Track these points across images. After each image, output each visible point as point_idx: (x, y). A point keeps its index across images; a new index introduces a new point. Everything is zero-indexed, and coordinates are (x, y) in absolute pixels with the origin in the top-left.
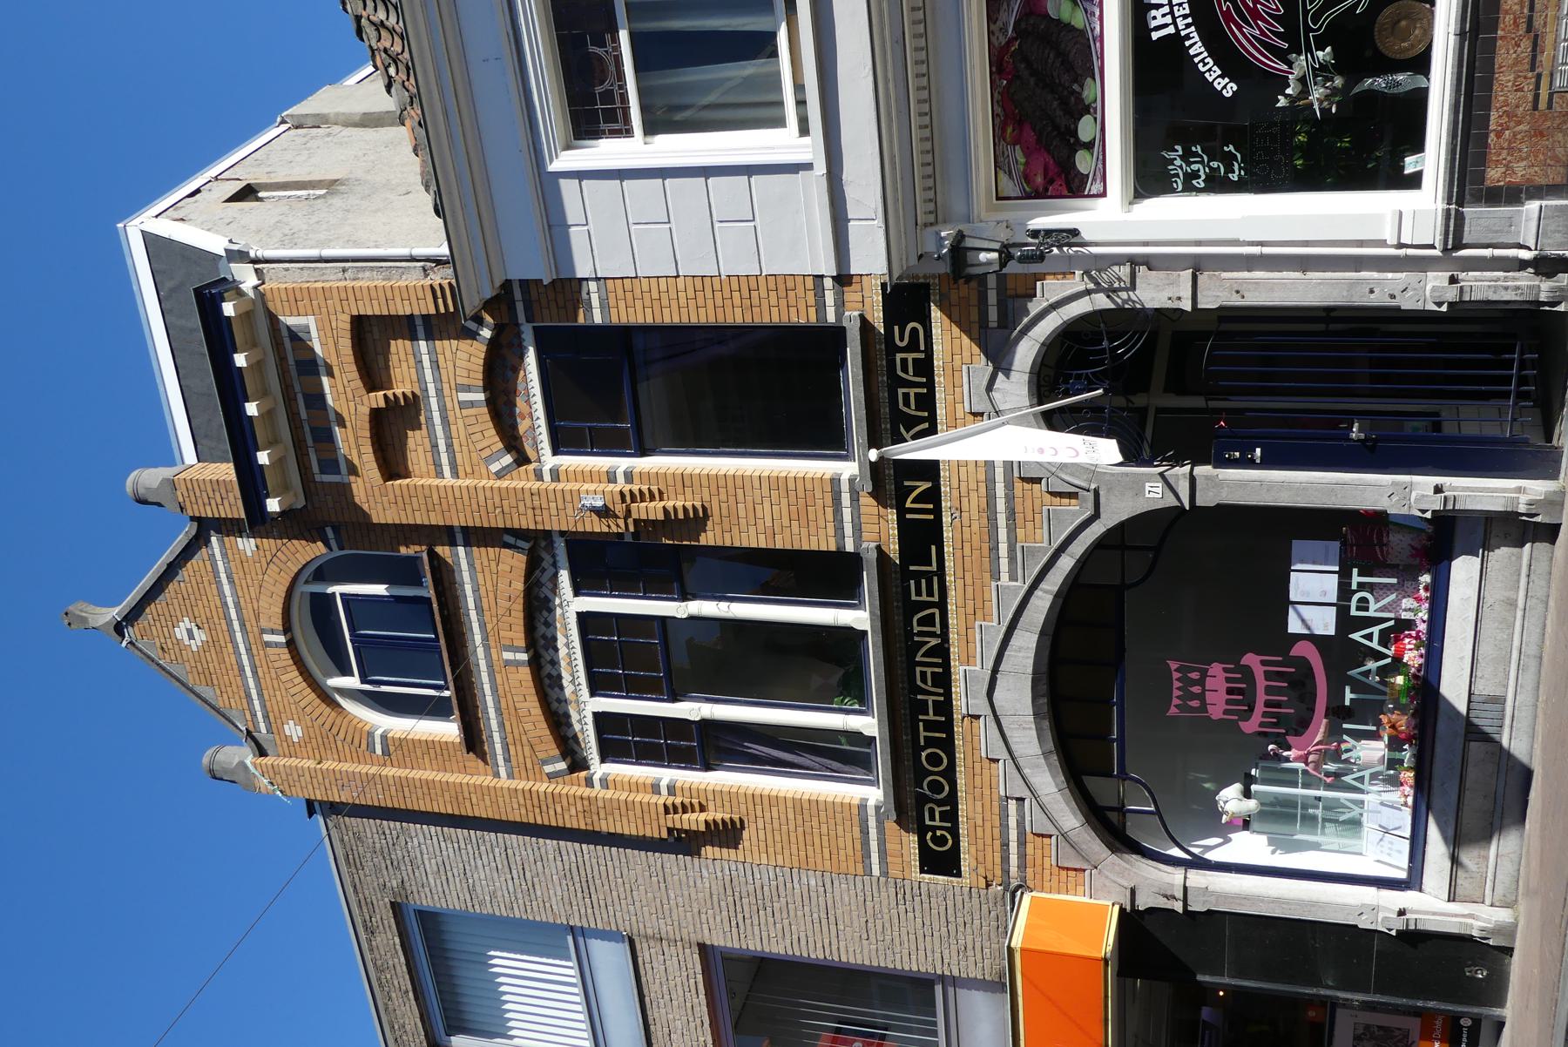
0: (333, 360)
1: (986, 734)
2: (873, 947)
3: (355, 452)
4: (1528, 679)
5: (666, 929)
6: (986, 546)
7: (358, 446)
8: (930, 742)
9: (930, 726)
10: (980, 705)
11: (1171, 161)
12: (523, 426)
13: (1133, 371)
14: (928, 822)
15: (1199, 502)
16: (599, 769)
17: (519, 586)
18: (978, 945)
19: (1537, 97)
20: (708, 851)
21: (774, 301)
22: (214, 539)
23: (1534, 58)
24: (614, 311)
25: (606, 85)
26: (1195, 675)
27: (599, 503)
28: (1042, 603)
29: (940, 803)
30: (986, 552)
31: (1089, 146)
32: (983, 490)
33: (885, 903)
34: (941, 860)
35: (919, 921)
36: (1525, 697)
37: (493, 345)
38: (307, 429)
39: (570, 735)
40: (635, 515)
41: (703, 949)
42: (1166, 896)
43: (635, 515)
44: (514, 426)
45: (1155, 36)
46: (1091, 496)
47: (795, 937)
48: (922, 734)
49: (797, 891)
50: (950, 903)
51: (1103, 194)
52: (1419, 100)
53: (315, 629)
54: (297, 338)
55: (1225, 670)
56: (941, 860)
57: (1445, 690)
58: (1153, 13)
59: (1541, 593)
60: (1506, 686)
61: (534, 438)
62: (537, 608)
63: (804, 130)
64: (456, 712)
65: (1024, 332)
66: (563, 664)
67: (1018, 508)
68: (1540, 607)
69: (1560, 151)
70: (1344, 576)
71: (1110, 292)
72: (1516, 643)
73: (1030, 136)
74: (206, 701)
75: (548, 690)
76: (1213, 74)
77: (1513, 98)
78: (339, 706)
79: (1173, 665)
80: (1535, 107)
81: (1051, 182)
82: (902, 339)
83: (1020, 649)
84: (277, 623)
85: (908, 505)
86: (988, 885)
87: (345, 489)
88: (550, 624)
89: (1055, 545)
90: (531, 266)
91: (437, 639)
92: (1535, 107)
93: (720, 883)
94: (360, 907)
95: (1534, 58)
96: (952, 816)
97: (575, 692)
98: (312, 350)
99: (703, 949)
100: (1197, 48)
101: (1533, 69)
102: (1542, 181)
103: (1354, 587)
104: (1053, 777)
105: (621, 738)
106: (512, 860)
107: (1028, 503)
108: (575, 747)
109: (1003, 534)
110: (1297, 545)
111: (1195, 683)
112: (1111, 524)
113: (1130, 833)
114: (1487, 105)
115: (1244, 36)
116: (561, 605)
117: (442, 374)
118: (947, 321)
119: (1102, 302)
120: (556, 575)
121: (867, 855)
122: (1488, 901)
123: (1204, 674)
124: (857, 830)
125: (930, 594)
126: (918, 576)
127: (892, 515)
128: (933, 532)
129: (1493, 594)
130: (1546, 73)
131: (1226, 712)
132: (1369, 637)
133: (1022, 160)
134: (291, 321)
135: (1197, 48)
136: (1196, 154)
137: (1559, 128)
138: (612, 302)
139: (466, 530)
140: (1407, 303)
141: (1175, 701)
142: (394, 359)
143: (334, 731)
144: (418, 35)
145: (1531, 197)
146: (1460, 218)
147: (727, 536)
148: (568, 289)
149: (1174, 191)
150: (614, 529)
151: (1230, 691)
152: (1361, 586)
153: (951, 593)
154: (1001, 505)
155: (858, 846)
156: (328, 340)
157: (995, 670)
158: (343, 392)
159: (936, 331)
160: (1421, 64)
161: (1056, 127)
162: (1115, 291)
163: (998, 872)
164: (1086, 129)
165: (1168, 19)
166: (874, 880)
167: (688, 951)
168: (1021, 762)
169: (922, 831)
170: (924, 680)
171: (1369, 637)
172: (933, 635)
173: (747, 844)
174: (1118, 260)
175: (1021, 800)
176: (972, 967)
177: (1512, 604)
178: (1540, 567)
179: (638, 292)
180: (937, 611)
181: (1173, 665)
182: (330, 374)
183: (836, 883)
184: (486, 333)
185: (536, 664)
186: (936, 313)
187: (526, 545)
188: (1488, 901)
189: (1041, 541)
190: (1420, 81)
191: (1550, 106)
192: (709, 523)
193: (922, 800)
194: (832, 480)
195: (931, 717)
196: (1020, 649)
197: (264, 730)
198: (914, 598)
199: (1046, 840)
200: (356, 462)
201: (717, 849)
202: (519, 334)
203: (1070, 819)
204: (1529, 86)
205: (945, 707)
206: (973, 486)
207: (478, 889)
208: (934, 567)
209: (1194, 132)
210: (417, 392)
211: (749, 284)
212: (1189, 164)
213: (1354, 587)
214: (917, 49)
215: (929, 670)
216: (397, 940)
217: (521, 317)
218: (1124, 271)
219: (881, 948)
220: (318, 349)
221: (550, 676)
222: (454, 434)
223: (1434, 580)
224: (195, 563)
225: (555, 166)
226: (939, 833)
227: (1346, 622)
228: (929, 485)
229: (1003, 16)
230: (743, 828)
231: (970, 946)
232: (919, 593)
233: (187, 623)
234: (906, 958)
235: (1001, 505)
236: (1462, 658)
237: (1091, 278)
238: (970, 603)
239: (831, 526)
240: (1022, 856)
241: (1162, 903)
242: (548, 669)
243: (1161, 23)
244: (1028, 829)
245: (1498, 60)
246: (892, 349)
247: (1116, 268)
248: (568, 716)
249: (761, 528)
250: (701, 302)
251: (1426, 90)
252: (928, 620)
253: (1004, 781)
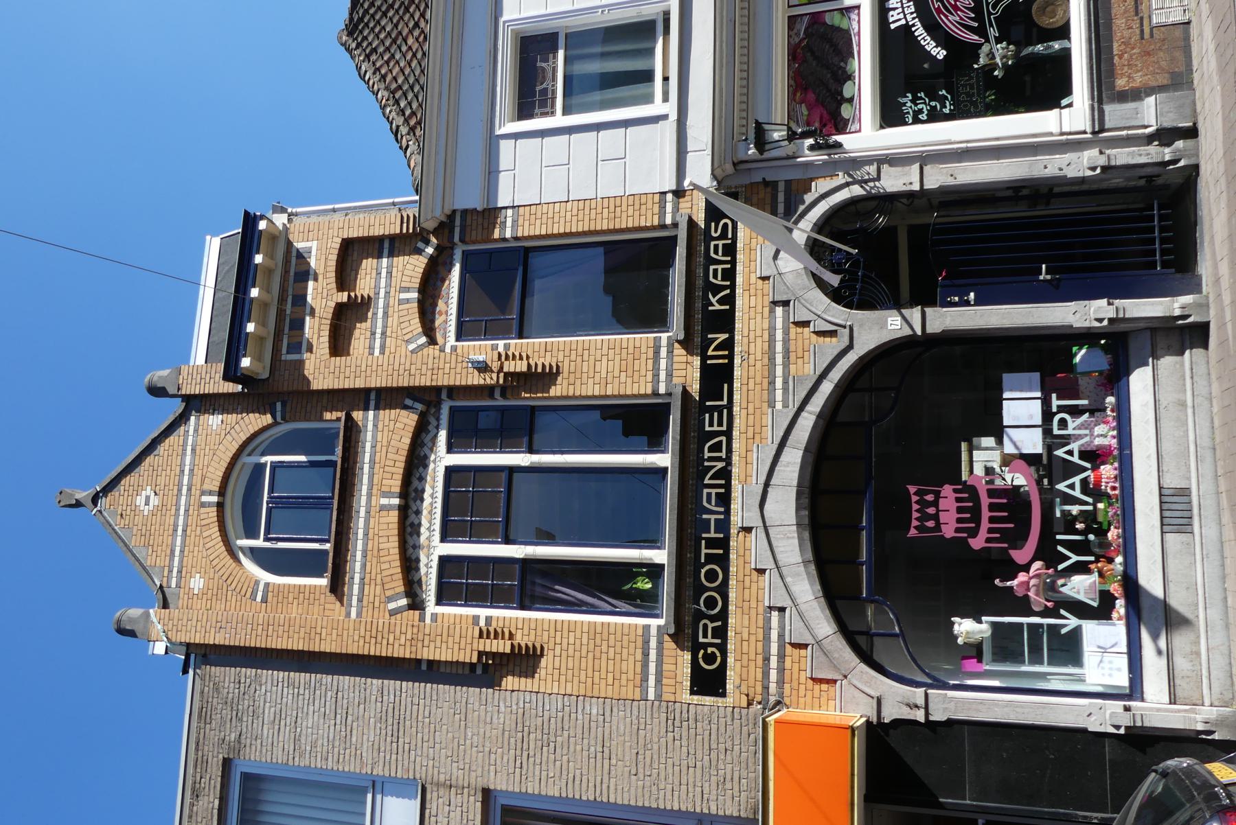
0: (320, 271)
1: (756, 541)
2: (640, 783)
3: (316, 336)
4: (1207, 468)
5: (458, 775)
7: (319, 336)
8: (710, 559)
9: (711, 543)
10: (753, 519)
11: (904, 104)
12: (438, 322)
13: (877, 249)
14: (701, 640)
15: (929, 330)
16: (431, 607)
17: (407, 441)
18: (736, 775)
19: (1142, 31)
20: (510, 682)
21: (630, 212)
22: (193, 418)
23: (1137, 8)
24: (520, 229)
25: (544, 86)
26: (930, 498)
27: (481, 358)
29: (712, 619)
30: (765, 385)
31: (850, 100)
33: (656, 730)
34: (709, 681)
35: (684, 749)
36: (1207, 486)
37: (432, 261)
38: (288, 321)
39: (416, 579)
40: (506, 369)
41: (487, 794)
42: (908, 705)
43: (506, 369)
44: (433, 321)
45: (893, 26)
46: (847, 331)
47: (571, 775)
48: (704, 551)
49: (580, 722)
50: (714, 727)
51: (860, 131)
52: (1065, 56)
53: (241, 501)
54: (301, 257)
55: (955, 491)
56: (709, 681)
57: (1143, 580)
58: (891, 13)
59: (1205, 391)
60: (1189, 479)
61: (445, 329)
62: (416, 462)
63: (666, 99)
64: (328, 574)
66: (425, 512)
67: (792, 348)
68: (1206, 403)
69: (1163, 64)
70: (1046, 403)
71: (862, 182)
72: (1191, 437)
73: (811, 96)
74: (138, 560)
75: (408, 538)
76: (930, 46)
77: (1126, 33)
78: (239, 561)
79: (912, 489)
80: (1142, 38)
81: (825, 125)
82: (716, 231)
84: (215, 486)
85: (710, 353)
86: (750, 704)
87: (301, 363)
88: (422, 479)
89: (818, 373)
90: (470, 200)
91: (332, 498)
92: (1142, 38)
93: (514, 717)
94: (196, 766)
95: (1137, 8)
96: (721, 632)
97: (428, 539)
98: (309, 264)
99: (487, 794)
100: (919, 31)
101: (1137, 14)
102: (1153, 84)
103: (1054, 409)
104: (811, 585)
105: (460, 581)
106: (339, 703)
107: (800, 342)
108: (418, 591)
109: (779, 370)
110: (1007, 378)
111: (930, 504)
112: (862, 353)
113: (875, 657)
114: (1110, 40)
115: (950, 22)
116: (434, 461)
117: (392, 281)
119: (857, 190)
120: (436, 436)
121: (645, 679)
122: (1207, 702)
123: (937, 495)
124: (639, 651)
125: (720, 424)
126: (711, 410)
127: (697, 361)
129: (1166, 398)
130: (1146, 16)
131: (957, 530)
132: (1072, 486)
133: (806, 113)
134: (299, 245)
135: (919, 31)
136: (921, 98)
137: (1160, 49)
138: (520, 222)
139: (379, 391)
140: (1071, 173)
141: (915, 523)
142: (362, 272)
143: (229, 582)
144: (436, 37)
145: (1149, 95)
146: (1102, 113)
147: (571, 387)
148: (491, 214)
149: (906, 124)
150: (489, 381)
151: (959, 510)
152: (1061, 409)
153: (737, 422)
154: (779, 347)
156: (320, 254)
157: (767, 485)
158: (322, 296)
160: (1063, 32)
161: (829, 90)
162: (866, 182)
163: (759, 689)
164: (847, 90)
165: (901, 16)
166: (649, 703)
167: (472, 799)
168: (785, 571)
169: (695, 648)
170: (709, 501)
171: (1072, 486)
172: (719, 459)
173: (543, 672)
174: (868, 161)
175: (782, 610)
176: (729, 802)
177: (1183, 404)
178: (1201, 369)
179: (539, 215)
180: (724, 439)
181: (912, 489)
182: (316, 279)
183: (615, 710)
184: (430, 250)
187: (420, 407)
188: (1207, 702)
189: (808, 369)
190: (1065, 43)
191: (1152, 35)
192: (560, 379)
193: (699, 615)
195: (712, 535)
197: (173, 585)
198: (707, 428)
199: (803, 652)
200: (315, 344)
201: (516, 679)
202: (452, 255)
203: (824, 626)
204: (1136, 25)
205: (724, 526)
206: (759, 333)
207: (303, 738)
208: (725, 402)
209: (915, 82)
210: (372, 295)
211: (615, 202)
212: (916, 105)
213: (1054, 409)
214: (742, 87)
215: (714, 491)
216: (217, 802)
217: (456, 239)
218: (872, 169)
219: (647, 784)
220: (313, 264)
221: (412, 525)
222: (389, 324)
223: (1118, 400)
224: (172, 440)
225: (498, 132)
226: (710, 650)
227: (1052, 441)
228: (727, 336)
229: (798, 26)
230: (542, 655)
231: (728, 777)
232: (711, 425)
233: (148, 491)
235: (779, 347)
236: (1149, 457)
237: (850, 176)
238: (751, 430)
239: (650, 374)
240: (781, 670)
241: (906, 714)
242: (412, 518)
243: (896, 19)
244: (787, 640)
245: (1113, 11)
246: (708, 238)
247: (867, 168)
248: (418, 560)
249: (597, 379)
250: (580, 217)
251: (1069, 49)
253: (769, 591)
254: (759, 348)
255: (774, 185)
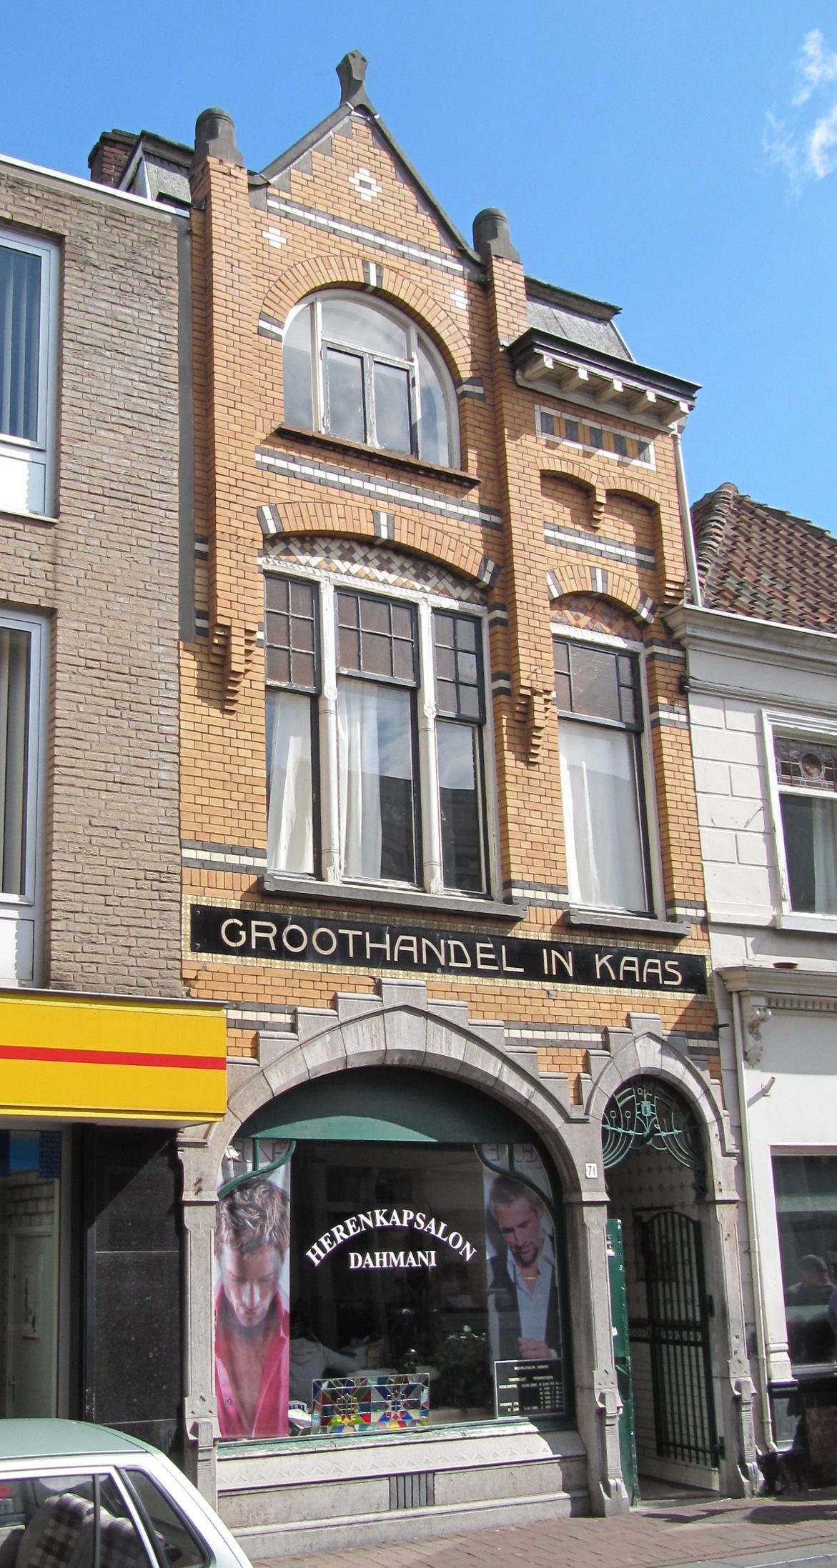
6: (527, 1018)
8: (343, 940)
9: (359, 942)
10: (392, 997)
28: (492, 1067)
29: (278, 939)
32: (573, 1021)
34: (208, 929)
56: (208, 929)
65: (688, 1066)
82: (671, 966)
83: (448, 1042)
96: (263, 950)
118: (686, 1005)
126: (496, 951)
128: (534, 972)
154: (563, 1036)
155: (216, 839)
157: (427, 1015)
159: (679, 995)
172: (448, 959)
173: (203, 711)
175: (293, 1028)
185: (369, 542)
186: (690, 997)
193: (281, 922)
194: (566, 887)
196: (448, 1042)
206: (576, 1012)
210: (599, 533)
226: (243, 933)
230: (224, 711)
232: (483, 950)
234: (68, 867)
235: (563, 1036)
252: (460, 958)
253: (314, 1013)
254: (558, 1011)
255: (715, 1036)
